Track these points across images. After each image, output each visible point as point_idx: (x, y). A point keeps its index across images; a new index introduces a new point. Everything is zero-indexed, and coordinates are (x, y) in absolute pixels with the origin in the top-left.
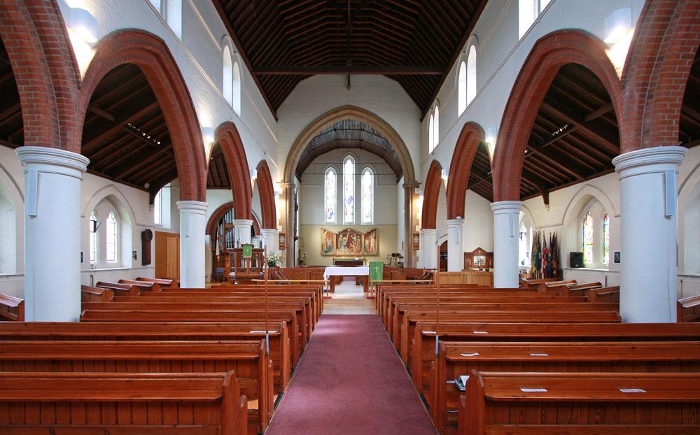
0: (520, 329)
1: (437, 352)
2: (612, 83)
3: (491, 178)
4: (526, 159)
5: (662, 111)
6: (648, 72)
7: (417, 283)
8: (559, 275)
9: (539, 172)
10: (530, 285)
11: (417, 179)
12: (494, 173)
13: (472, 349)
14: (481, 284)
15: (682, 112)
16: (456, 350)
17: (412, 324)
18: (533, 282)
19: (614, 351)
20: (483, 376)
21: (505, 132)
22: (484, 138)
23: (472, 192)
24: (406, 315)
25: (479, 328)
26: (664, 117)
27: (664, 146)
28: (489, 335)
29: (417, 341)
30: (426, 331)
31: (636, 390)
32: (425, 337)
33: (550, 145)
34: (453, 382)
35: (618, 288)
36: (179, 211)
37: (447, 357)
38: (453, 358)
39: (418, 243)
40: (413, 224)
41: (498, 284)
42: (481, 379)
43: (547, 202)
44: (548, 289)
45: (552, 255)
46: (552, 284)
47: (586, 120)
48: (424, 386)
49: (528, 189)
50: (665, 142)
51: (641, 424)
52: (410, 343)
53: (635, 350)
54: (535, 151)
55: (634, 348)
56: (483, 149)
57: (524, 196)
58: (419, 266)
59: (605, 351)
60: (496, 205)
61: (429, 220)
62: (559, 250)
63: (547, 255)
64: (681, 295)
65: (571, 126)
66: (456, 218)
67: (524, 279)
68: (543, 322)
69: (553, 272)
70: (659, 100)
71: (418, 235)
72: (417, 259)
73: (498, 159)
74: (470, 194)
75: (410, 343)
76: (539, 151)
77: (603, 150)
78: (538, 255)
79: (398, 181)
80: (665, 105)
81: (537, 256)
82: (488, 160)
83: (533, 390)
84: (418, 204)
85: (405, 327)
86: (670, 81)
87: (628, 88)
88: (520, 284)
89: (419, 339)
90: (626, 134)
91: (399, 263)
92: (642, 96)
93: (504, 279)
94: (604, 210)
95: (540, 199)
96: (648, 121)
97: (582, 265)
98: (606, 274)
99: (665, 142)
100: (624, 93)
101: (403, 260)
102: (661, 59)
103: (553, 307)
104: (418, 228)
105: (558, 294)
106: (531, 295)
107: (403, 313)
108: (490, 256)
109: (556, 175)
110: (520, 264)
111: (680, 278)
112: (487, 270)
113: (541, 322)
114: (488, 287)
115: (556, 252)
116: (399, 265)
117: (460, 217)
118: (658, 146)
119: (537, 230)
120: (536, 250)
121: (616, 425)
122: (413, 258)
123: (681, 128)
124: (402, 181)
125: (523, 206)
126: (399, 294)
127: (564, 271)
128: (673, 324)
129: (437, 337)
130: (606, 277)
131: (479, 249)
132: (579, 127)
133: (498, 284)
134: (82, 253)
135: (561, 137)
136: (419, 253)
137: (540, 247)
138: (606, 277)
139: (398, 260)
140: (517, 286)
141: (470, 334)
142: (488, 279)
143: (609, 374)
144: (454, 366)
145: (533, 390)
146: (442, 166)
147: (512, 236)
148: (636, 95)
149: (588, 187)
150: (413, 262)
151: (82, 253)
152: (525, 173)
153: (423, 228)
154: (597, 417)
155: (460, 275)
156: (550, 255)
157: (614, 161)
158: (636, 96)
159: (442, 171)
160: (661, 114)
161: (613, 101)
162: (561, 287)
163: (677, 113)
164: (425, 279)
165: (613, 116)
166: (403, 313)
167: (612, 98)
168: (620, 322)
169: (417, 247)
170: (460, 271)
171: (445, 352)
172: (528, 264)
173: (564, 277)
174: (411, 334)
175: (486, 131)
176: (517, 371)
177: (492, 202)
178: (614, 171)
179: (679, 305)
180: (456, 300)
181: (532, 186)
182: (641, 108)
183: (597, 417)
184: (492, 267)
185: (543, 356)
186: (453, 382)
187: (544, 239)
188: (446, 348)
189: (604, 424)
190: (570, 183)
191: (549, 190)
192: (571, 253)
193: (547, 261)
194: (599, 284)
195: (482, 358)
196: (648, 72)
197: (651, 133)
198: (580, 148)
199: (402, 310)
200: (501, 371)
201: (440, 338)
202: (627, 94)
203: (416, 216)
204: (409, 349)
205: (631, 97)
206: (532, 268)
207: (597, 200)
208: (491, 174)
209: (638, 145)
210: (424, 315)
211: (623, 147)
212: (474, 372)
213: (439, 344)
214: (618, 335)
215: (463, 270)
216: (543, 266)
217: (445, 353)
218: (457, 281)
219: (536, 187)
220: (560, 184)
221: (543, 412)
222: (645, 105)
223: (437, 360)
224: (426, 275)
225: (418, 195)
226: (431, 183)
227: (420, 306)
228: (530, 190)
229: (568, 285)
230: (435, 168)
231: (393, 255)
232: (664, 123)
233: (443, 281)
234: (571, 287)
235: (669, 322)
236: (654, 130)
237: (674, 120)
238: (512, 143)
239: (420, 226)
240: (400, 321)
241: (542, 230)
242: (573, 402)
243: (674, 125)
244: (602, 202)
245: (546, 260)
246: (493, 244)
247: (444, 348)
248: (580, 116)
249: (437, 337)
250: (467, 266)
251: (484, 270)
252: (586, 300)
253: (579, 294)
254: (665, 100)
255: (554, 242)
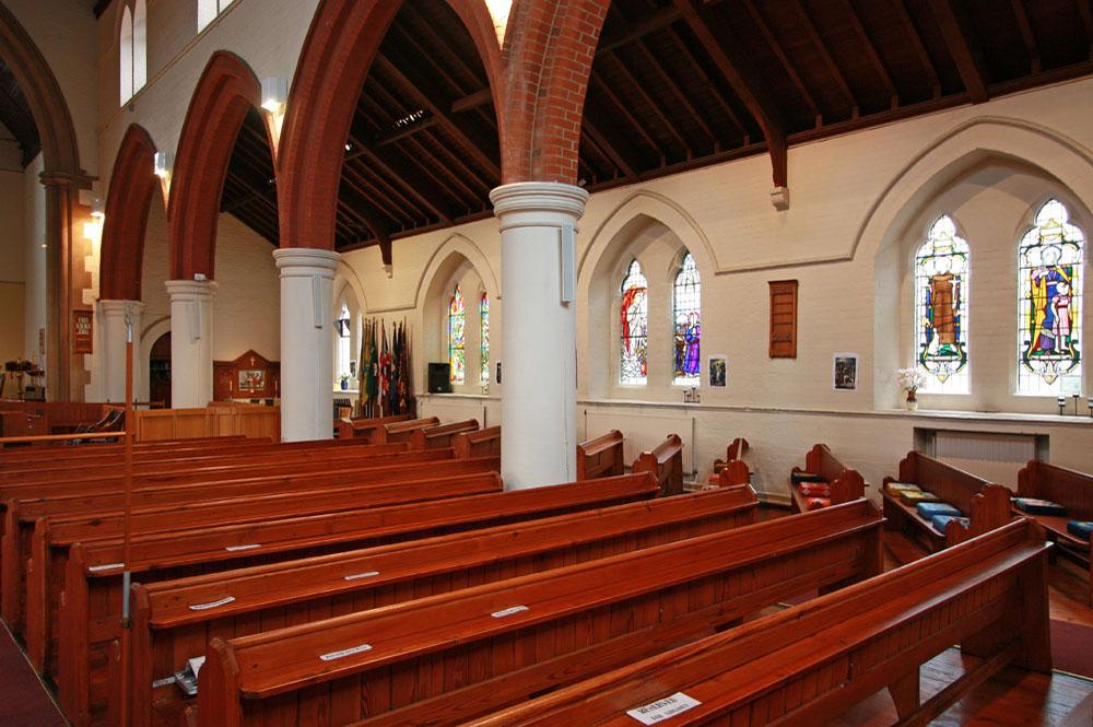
0: (329, 528)
1: (126, 615)
2: (490, 50)
3: (275, 193)
4: (347, 162)
5: (557, 122)
6: (541, 49)
7: (85, 441)
8: (410, 409)
9: (373, 195)
10: (357, 432)
11: (87, 164)
12: (281, 180)
13: (219, 589)
14: (254, 434)
15: (583, 128)
16: (177, 598)
17: (59, 552)
18: (364, 425)
19: (487, 544)
20: (237, 648)
21: (302, 92)
22: (260, 102)
23: (235, 220)
24: (40, 530)
25: (241, 538)
26: (559, 132)
27: (560, 181)
28: (263, 551)
29: (72, 597)
30: (99, 564)
31: (515, 610)
32: (97, 583)
33: (392, 144)
34: (171, 680)
35: (497, 430)
36: (278, 271)
37: (152, 621)
38: (168, 621)
39: (90, 336)
40: (74, 285)
41: (292, 431)
42: (232, 658)
43: (387, 259)
44: (391, 437)
45: (397, 370)
46: (398, 426)
47: (454, 110)
48: (92, 710)
49: (352, 228)
50: (562, 175)
51: (525, 665)
52: (52, 604)
53: (519, 537)
54: (365, 151)
55: (516, 534)
56: (258, 122)
57: (346, 240)
58: (93, 395)
59: (472, 548)
60: (283, 255)
61: (121, 272)
62: (410, 359)
63: (389, 368)
64: (581, 434)
65: (428, 115)
66: (193, 279)
67: (346, 420)
68: (375, 507)
69: (399, 401)
70: (554, 102)
71: (88, 313)
72: (86, 377)
73: (289, 154)
74: (227, 222)
75: (52, 604)
76: (371, 150)
77: (479, 173)
78: (371, 369)
79: (27, 159)
80: (560, 113)
81: (371, 370)
82: (268, 149)
83: (345, 653)
84: (89, 232)
85: (37, 564)
86: (567, 75)
87: (512, 67)
88: (336, 430)
89: (81, 588)
90: (510, 153)
91: (28, 389)
92: (532, 88)
93: (303, 420)
94: (482, 284)
95: (763, 163)
96: (540, 134)
97: (448, 388)
98: (485, 403)
99: (562, 175)
100: (507, 76)
101: (42, 382)
102: (556, 32)
103: (394, 473)
104: (90, 295)
105: (405, 447)
106: (355, 452)
107: (31, 526)
108: (273, 369)
109: (403, 207)
110: (337, 388)
111: (584, 407)
112: (269, 403)
113: (371, 507)
114: (269, 439)
115: (404, 362)
116: (31, 395)
117: (202, 277)
118: (552, 181)
119: (370, 317)
120: (368, 358)
121: (487, 682)
122: (74, 374)
123: (581, 155)
124: (40, 164)
125: (344, 262)
126: (21, 475)
127: (419, 401)
128: (570, 485)
129: (127, 575)
130: (485, 408)
131: (252, 353)
132: (440, 119)
133: (292, 431)
134: (499, 381)
135: (411, 132)
136: (92, 361)
137: (376, 352)
138: (485, 408)
139: (27, 380)
140: (329, 435)
141: (218, 556)
142: (268, 421)
143: (391, 607)
144: (168, 639)
145: (345, 653)
146: (158, 144)
147: (320, 327)
148: (524, 83)
149: (457, 239)
150: (73, 387)
151: (499, 381)
152: (345, 191)
153: (102, 296)
154: (458, 676)
155: (203, 416)
156: (393, 368)
157: (493, 193)
158: (524, 86)
159: (157, 156)
160: (556, 127)
161: (491, 84)
162: (412, 431)
163: (576, 131)
164: (108, 430)
165: (490, 109)
166: (31, 526)
167: (490, 78)
168: (501, 490)
169: (85, 345)
170: (203, 405)
171: (150, 609)
172: (354, 391)
173: (419, 412)
174: (54, 579)
175: (263, 83)
176: (320, 619)
177: (278, 246)
178: (492, 215)
179: (580, 451)
180: (188, 478)
181: (361, 223)
182: (530, 108)
183: (458, 676)
184: (279, 396)
185: (371, 575)
186: (171, 680)
187: (384, 337)
188: (149, 598)
189: (468, 684)
190: (428, 227)
191: (392, 236)
192: (430, 365)
193: (389, 380)
194: (474, 423)
195: (388, 578)
196: (541, 49)
197: (544, 156)
198: (439, 156)
199: (28, 519)
200: (433, 595)
201: (134, 577)
202: (511, 77)
203: (82, 264)
204: (51, 620)
205: (517, 85)
206: (361, 395)
207: (471, 266)
208: (274, 185)
209: (527, 175)
210: (96, 523)
211: (505, 172)
212: (216, 642)
213: (132, 592)
214: (496, 515)
215: (210, 404)
216: (381, 392)
217: (149, 613)
218: (197, 430)
219: (369, 227)
220: (424, 224)
221: (366, 694)
222: (535, 104)
223: (126, 634)
224: (111, 418)
225: (88, 209)
226: (899, 301)
227: (89, 501)
228: (356, 230)
229: (424, 427)
230: (138, 144)
231: (11, 366)
232: (559, 142)
233: (160, 432)
234: (429, 432)
235: (566, 482)
236: (547, 152)
237: (573, 142)
238: (318, 125)
239: (95, 290)
240: (24, 548)
241: (379, 317)
242: (419, 657)
243: (572, 150)
244: (479, 270)
245: (387, 378)
246: (277, 349)
247: (145, 599)
248: (444, 99)
249: (127, 575)
250: (220, 394)
251: (262, 402)
252: (451, 455)
253: (441, 440)
254: (561, 103)
255: (401, 341)
